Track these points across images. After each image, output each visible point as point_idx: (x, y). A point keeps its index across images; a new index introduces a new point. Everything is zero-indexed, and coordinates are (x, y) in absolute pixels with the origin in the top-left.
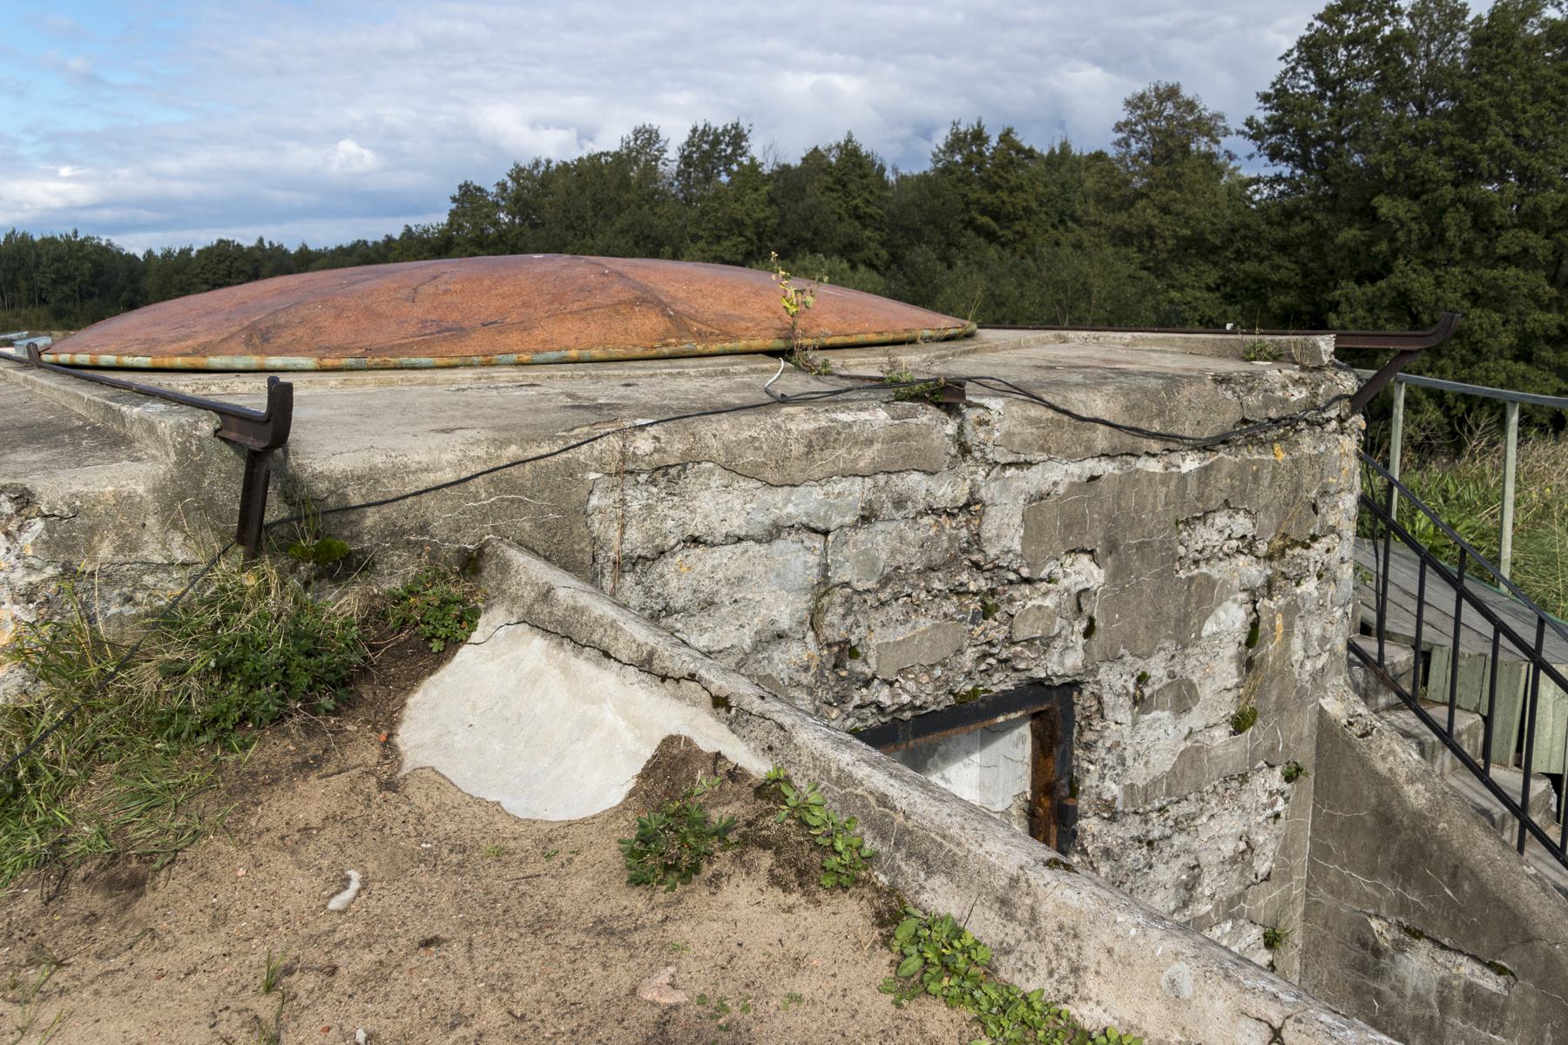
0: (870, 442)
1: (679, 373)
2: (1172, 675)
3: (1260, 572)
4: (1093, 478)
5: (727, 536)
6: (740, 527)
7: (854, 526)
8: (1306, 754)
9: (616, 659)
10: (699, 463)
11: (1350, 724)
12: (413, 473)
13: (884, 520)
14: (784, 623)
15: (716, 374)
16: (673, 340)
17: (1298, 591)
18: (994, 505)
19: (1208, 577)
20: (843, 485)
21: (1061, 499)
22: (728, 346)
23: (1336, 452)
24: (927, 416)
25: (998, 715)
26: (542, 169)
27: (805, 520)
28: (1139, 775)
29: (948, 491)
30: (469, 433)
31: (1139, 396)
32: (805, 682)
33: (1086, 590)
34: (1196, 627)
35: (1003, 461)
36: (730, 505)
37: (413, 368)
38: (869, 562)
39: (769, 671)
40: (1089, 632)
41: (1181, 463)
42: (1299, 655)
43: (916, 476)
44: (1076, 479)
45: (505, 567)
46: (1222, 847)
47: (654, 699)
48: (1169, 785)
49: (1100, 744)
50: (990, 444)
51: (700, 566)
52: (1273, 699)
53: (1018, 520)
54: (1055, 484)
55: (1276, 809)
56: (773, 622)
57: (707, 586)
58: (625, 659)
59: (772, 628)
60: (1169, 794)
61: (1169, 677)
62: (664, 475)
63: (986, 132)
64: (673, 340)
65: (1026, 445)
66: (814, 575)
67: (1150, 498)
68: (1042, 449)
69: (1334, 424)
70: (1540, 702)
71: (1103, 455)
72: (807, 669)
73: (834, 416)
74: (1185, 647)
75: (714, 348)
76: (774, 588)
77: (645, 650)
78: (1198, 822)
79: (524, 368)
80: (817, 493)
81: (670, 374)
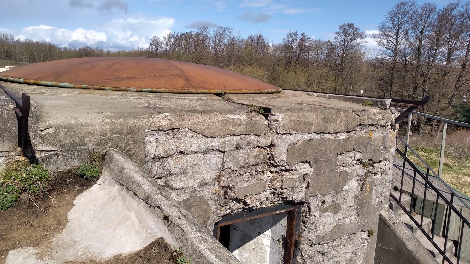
0: (240, 125)
1: (186, 98)
2: (333, 201)
3: (363, 171)
4: (311, 140)
5: (191, 151)
6: (196, 149)
7: (233, 150)
8: (375, 228)
9: (138, 197)
10: (184, 128)
11: (390, 220)
12: (84, 126)
13: (243, 149)
14: (209, 180)
15: (198, 99)
16: (186, 88)
17: (375, 177)
18: (278, 146)
19: (346, 172)
20: (230, 138)
21: (300, 145)
22: (203, 91)
23: (389, 135)
24: (260, 118)
25: (277, 211)
26: (176, 34)
27: (217, 148)
28: (321, 231)
29: (263, 141)
30: (107, 114)
31: (327, 115)
32: (214, 198)
33: (307, 174)
34: (342, 187)
35: (282, 133)
36: (193, 142)
37: (104, 90)
38: (236, 161)
39: (202, 195)
40: (307, 187)
41: (340, 136)
42: (374, 197)
43: (254, 136)
44: (305, 140)
45: (112, 158)
46: (347, 256)
47: (147, 213)
48: (330, 236)
49: (309, 222)
50: (278, 128)
51: (182, 160)
52: (365, 210)
53: (286, 151)
54: (299, 141)
55: (364, 244)
56: (205, 179)
57: (184, 167)
58: (141, 197)
59: (204, 181)
60: (330, 238)
61: (332, 202)
62: (172, 131)
63: (298, 33)
64: (186, 88)
65: (290, 128)
66: (219, 165)
67: (329, 147)
68: (295, 130)
69: (389, 126)
70: (451, 217)
71: (314, 133)
72: (215, 194)
73: (229, 116)
74: (338, 193)
75: (199, 91)
76: (206, 168)
77: (147, 195)
78: (339, 247)
79: (138, 93)
80: (222, 140)
81: (183, 98)
